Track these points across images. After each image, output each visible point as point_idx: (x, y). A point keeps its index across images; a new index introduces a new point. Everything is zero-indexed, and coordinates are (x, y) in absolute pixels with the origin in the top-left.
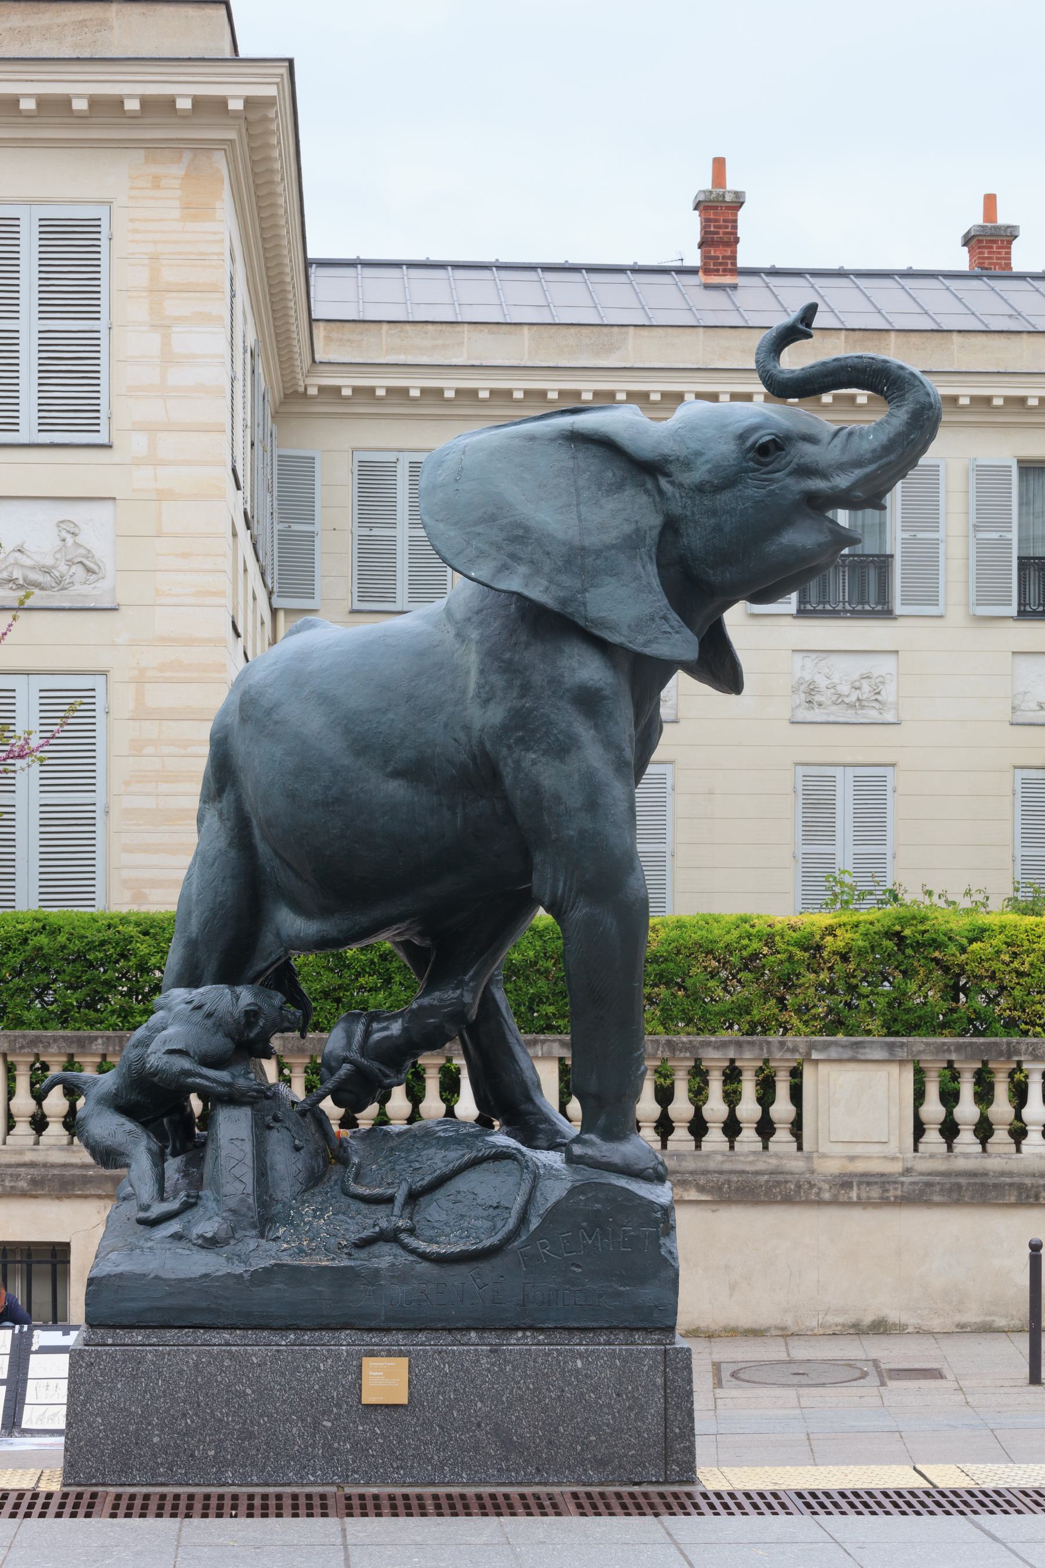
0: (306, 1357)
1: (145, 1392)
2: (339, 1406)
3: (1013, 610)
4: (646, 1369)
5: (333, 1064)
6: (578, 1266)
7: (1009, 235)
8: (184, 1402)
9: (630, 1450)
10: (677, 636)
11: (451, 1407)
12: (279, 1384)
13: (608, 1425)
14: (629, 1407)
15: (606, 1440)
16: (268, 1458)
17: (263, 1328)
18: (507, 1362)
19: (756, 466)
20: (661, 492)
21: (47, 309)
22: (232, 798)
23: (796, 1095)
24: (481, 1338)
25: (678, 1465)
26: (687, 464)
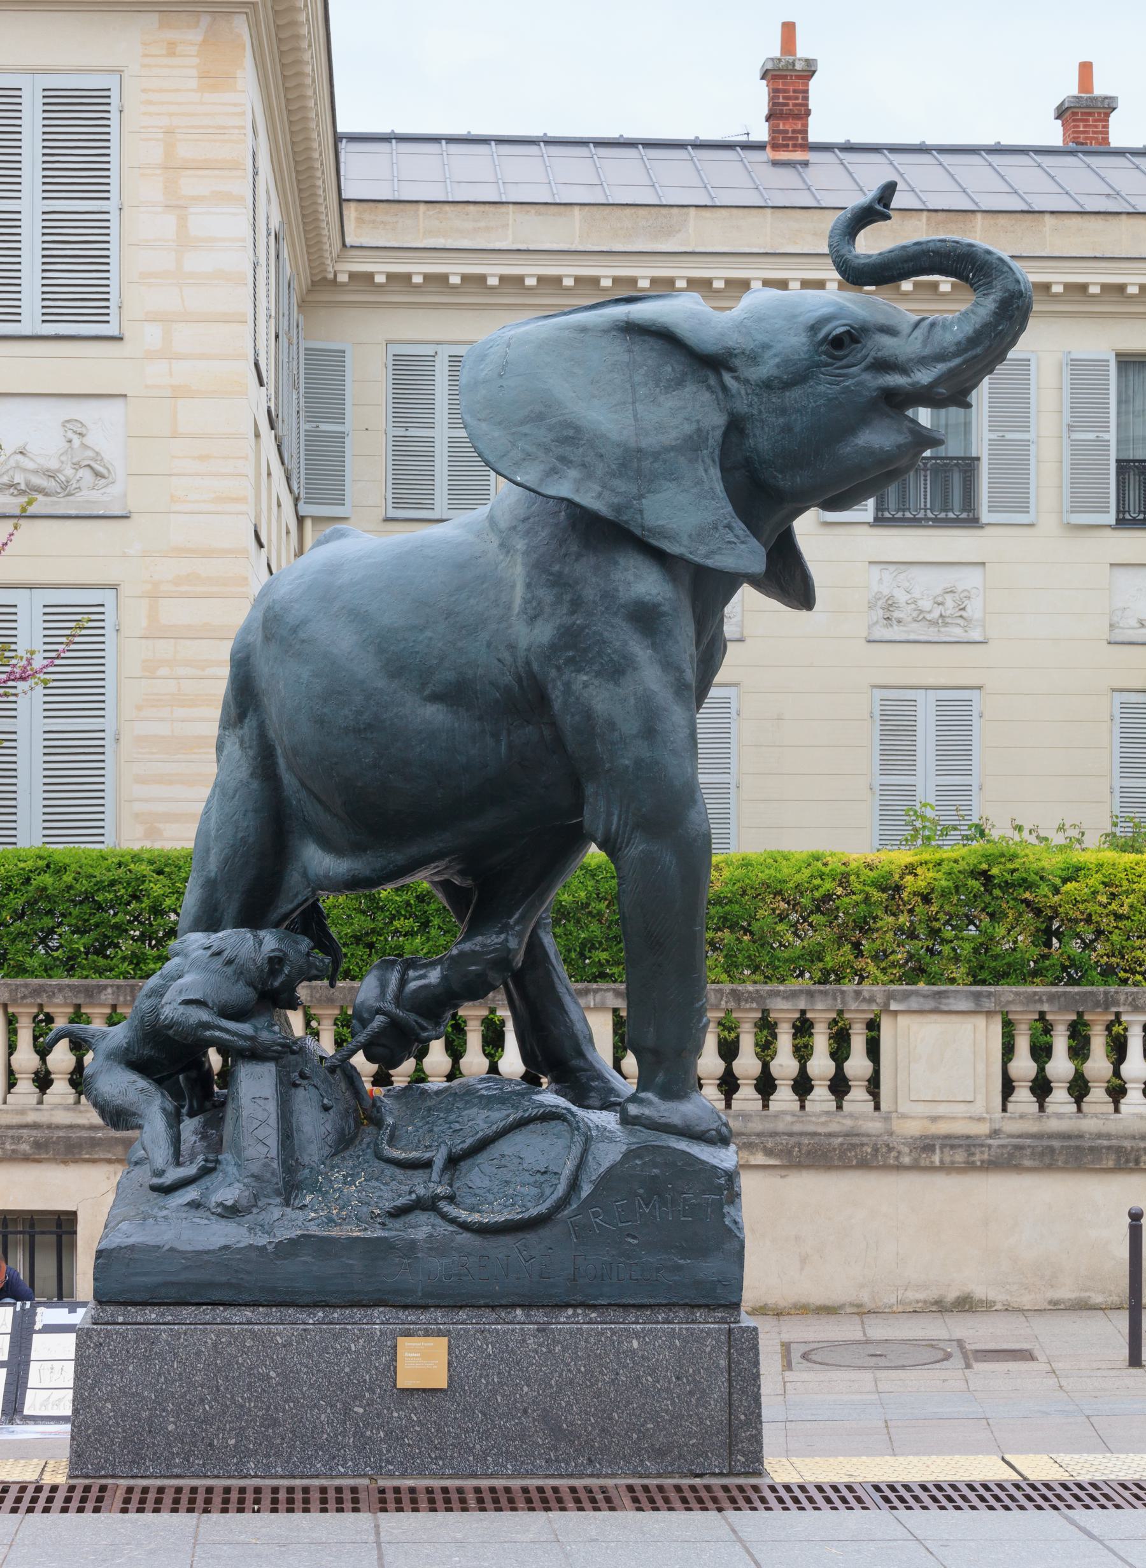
0: (336, 1336)
1: (159, 1375)
4: (708, 1349)
5: (366, 1015)
6: (634, 1237)
7: (1105, 108)
8: (202, 1386)
9: (691, 1438)
10: (743, 546)
11: (494, 1392)
12: (307, 1366)
14: (690, 1392)
15: (665, 1428)
16: (293, 1447)
17: (288, 1305)
19: (830, 360)
20: (725, 388)
21: (52, 188)
22: (254, 723)
23: (873, 1050)
24: (527, 1316)
25: (744, 1455)
26: (753, 358)
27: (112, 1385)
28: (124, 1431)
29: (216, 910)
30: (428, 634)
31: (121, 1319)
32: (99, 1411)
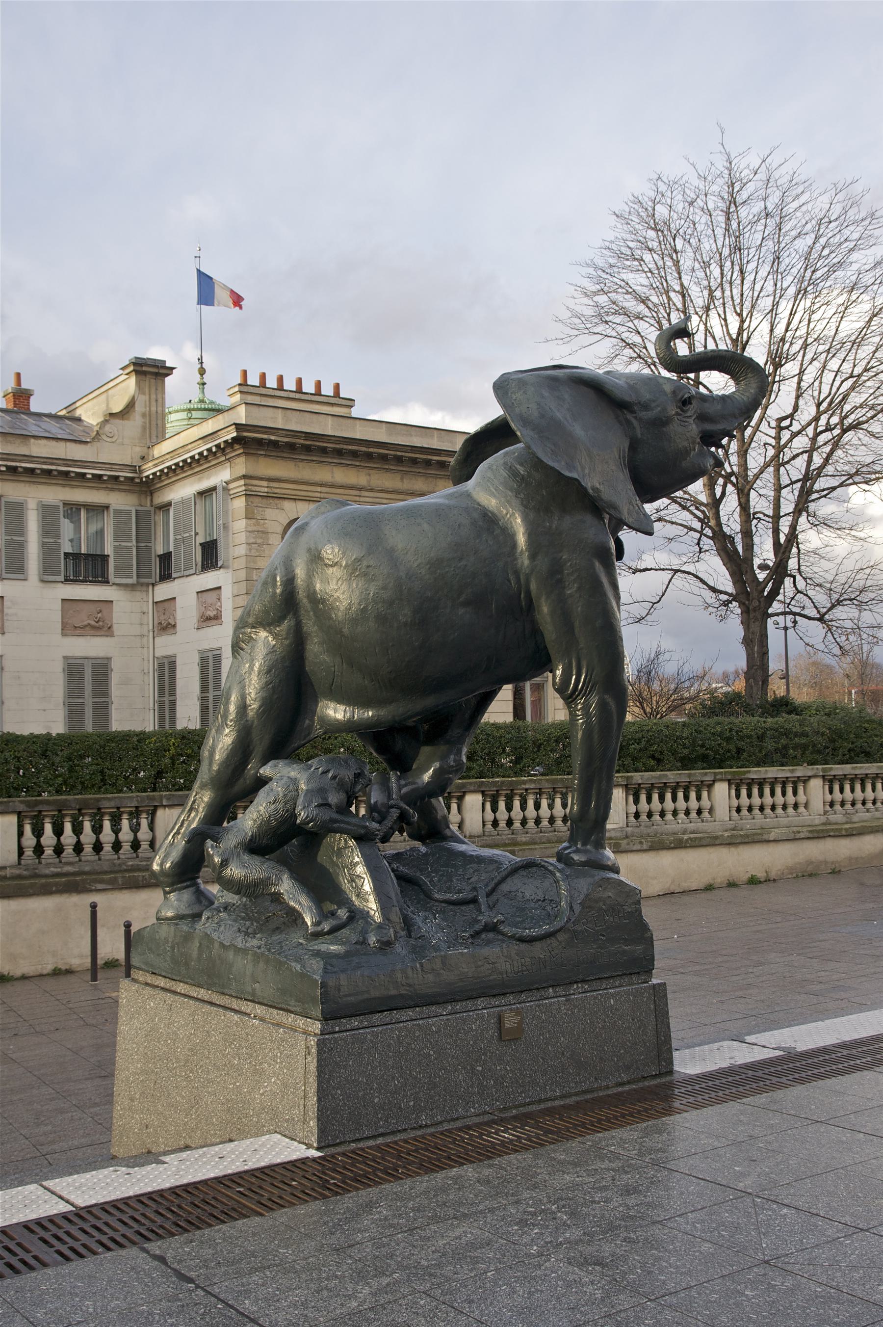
0: (464, 1021)
1: (368, 1064)
2: (485, 1054)
3: (62, 578)
5: (383, 809)
6: (603, 936)
8: (392, 1068)
13: (629, 1041)
16: (446, 1101)
17: (432, 1004)
18: (575, 1007)
20: (628, 422)
22: (293, 623)
26: (646, 407)
27: (340, 1077)
28: (349, 1108)
29: (248, 746)
30: (463, 563)
31: (337, 1029)
32: (333, 1097)
